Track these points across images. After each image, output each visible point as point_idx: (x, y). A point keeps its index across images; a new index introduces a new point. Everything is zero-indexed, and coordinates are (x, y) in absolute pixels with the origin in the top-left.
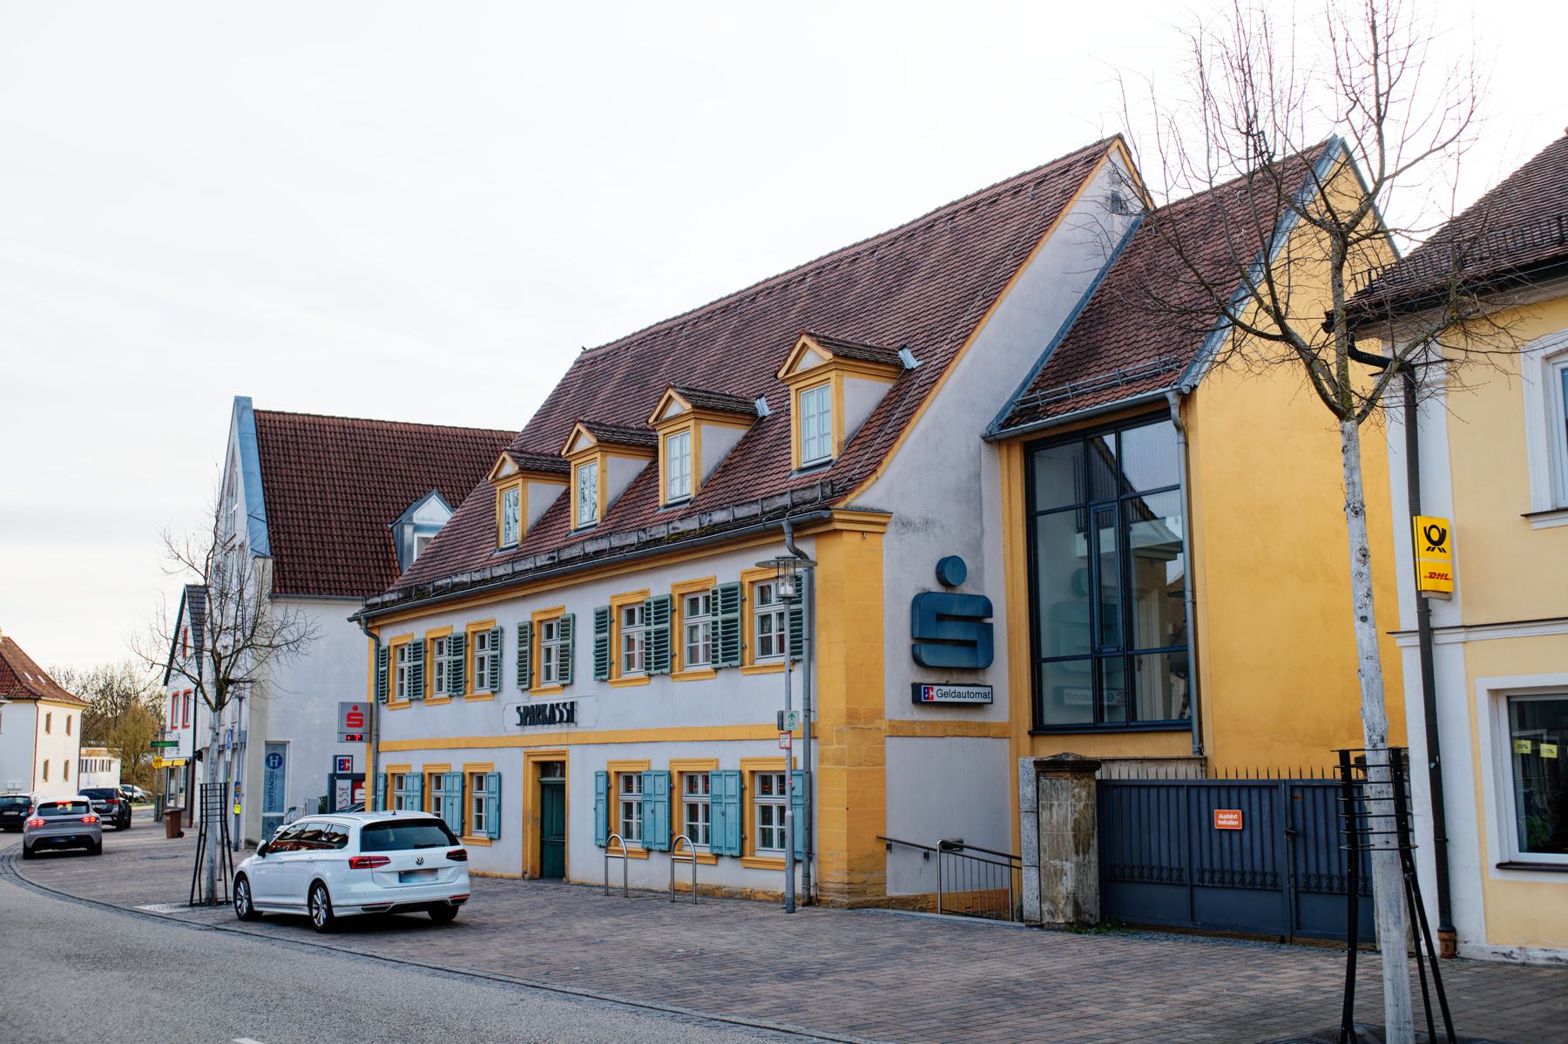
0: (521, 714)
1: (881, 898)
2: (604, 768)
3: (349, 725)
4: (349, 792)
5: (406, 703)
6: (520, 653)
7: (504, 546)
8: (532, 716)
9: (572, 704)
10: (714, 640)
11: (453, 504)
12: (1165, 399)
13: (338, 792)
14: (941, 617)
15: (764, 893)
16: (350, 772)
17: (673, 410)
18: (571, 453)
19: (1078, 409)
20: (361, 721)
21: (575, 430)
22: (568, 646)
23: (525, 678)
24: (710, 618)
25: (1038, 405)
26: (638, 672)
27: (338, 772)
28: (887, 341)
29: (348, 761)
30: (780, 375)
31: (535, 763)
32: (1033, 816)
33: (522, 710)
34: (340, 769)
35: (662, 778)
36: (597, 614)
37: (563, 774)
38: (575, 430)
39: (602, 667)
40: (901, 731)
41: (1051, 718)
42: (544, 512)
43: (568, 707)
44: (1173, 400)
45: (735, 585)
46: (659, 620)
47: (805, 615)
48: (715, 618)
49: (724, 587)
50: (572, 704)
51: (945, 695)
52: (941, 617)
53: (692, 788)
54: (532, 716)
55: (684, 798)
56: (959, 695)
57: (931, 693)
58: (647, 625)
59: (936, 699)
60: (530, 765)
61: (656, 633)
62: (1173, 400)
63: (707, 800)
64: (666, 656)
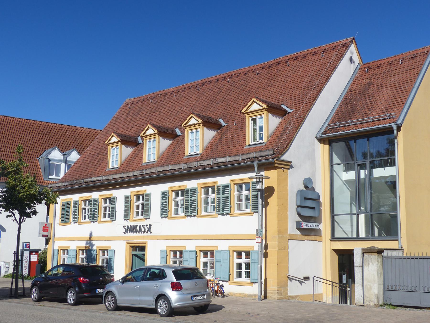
0: (125, 229)
1: (286, 296)
2: (165, 248)
3: (43, 231)
4: (28, 256)
5: (88, 222)
6: (125, 206)
7: (111, 168)
8: (129, 229)
9: (150, 225)
10: (90, 213)
11: (80, 153)
12: (392, 128)
13: (24, 256)
14: (306, 199)
15: (239, 294)
16: (29, 248)
17: (193, 121)
18: (144, 135)
19: (354, 129)
20: (48, 230)
21: (111, 136)
22: (114, 207)
23: (127, 216)
24: (184, 198)
25: (337, 127)
26: (181, 213)
27: (24, 248)
28: (171, 126)
29: (28, 244)
30: (243, 111)
31: (131, 246)
32: (361, 268)
33: (126, 228)
34: (25, 247)
35: (193, 253)
36: (163, 193)
37: (145, 251)
38: (111, 136)
39: (164, 212)
40: (293, 238)
41: (338, 234)
42: (128, 156)
43: (148, 227)
44: (395, 128)
45: (228, 185)
46: (94, 206)
47: (150, 204)
48: (187, 199)
49: (224, 185)
50: (150, 225)
51: (306, 225)
52: (306, 199)
53: (175, 256)
54: (129, 229)
55: (235, 260)
56: (310, 226)
57: (303, 225)
58: (91, 206)
59: (304, 227)
60: (129, 247)
61: (191, 201)
62: (395, 128)
63: (213, 260)
64: (166, 211)
